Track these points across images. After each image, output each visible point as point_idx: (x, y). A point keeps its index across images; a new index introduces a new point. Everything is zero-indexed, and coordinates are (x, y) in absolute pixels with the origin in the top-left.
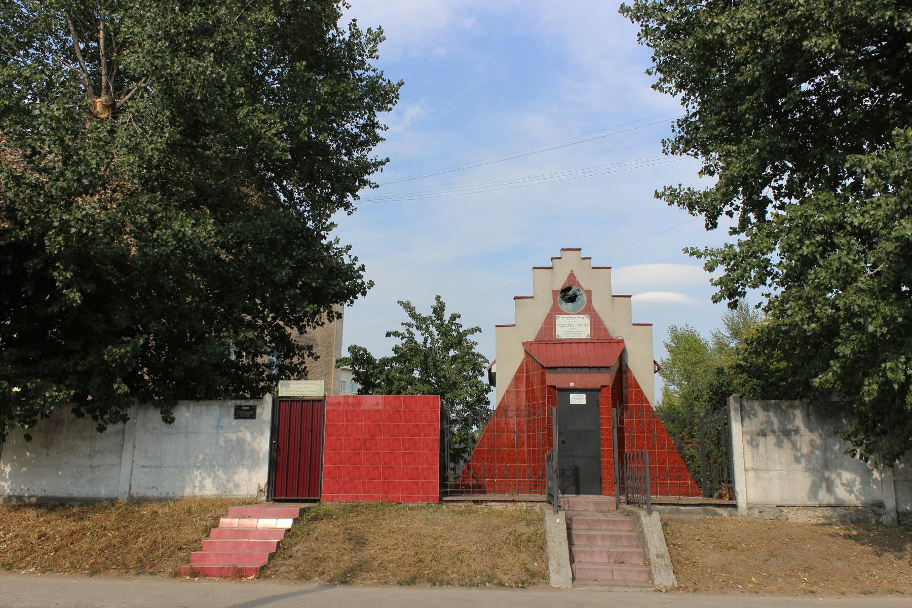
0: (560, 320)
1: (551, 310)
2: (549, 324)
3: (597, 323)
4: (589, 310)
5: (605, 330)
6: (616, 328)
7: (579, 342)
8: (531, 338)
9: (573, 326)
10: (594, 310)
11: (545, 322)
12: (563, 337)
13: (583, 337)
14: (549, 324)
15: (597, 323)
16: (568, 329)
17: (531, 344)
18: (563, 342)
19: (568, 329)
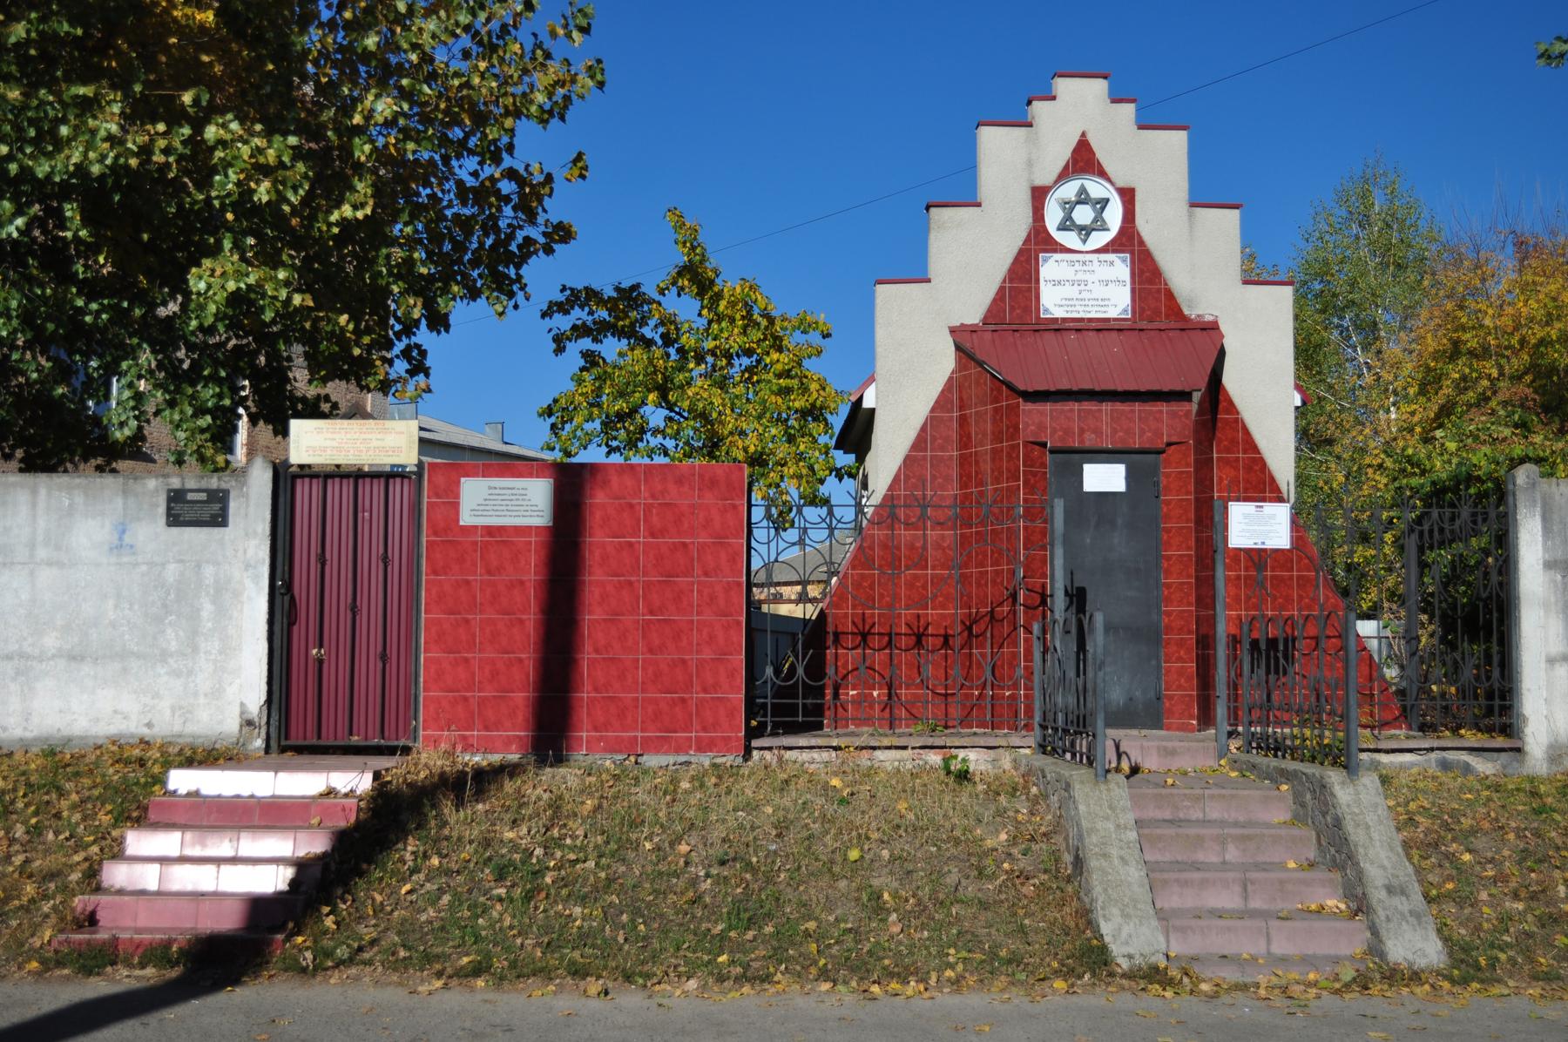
0: (1051, 268)
1: (1027, 240)
4: (1128, 241)
10: (1142, 243)
11: (1016, 260)
12: (1059, 313)
16: (1070, 291)
18: (1060, 327)
19: (1070, 291)
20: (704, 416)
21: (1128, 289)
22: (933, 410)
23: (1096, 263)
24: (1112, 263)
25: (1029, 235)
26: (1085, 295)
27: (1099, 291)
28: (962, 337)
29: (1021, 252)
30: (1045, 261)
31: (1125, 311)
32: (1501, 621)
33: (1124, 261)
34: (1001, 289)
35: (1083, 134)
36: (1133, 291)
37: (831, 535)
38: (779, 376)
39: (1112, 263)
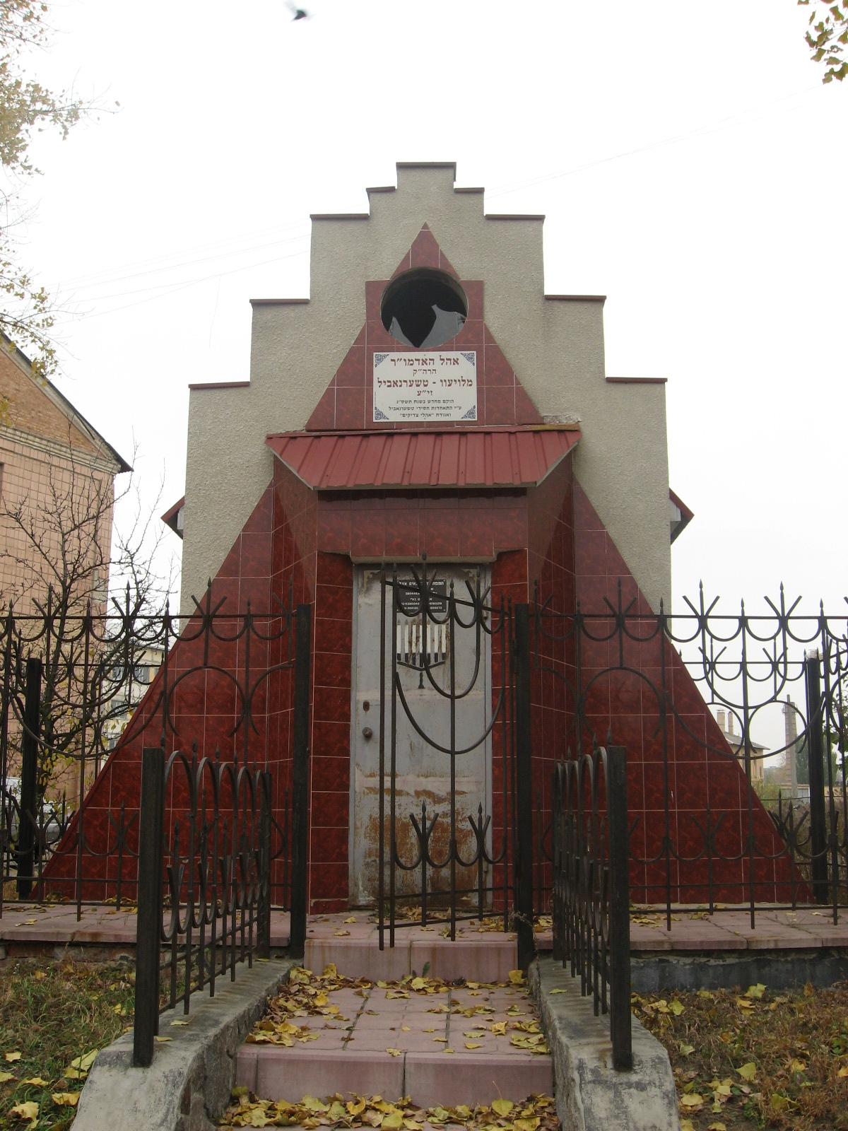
1: (359, 339)
2: (354, 377)
3: (496, 376)
5: (523, 396)
6: (556, 401)
7: (439, 432)
8: (297, 421)
9: (426, 386)
10: (490, 338)
12: (394, 417)
13: (456, 416)
14: (354, 377)
15: (496, 376)
16: (408, 393)
17: (293, 437)
18: (390, 432)
20: (251, 1119)
21: (474, 388)
22: (246, 528)
23: (437, 361)
24: (456, 361)
25: (363, 331)
26: (425, 396)
27: (440, 392)
28: (281, 442)
29: (352, 352)
30: (380, 360)
31: (470, 413)
32: (503, 703)
33: (470, 359)
34: (329, 392)
35: (425, 226)
36: (479, 391)
37: (703, 626)
38: (11, 32)
39: (456, 361)
